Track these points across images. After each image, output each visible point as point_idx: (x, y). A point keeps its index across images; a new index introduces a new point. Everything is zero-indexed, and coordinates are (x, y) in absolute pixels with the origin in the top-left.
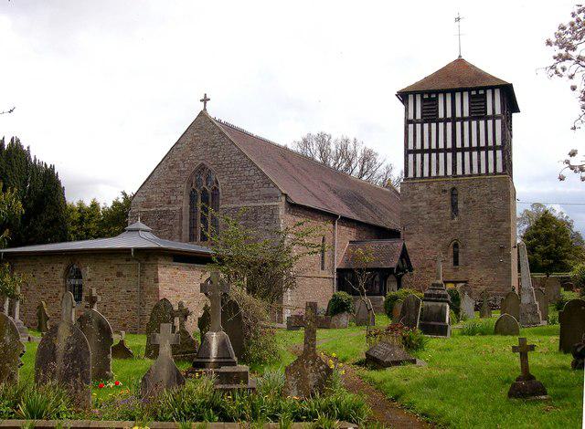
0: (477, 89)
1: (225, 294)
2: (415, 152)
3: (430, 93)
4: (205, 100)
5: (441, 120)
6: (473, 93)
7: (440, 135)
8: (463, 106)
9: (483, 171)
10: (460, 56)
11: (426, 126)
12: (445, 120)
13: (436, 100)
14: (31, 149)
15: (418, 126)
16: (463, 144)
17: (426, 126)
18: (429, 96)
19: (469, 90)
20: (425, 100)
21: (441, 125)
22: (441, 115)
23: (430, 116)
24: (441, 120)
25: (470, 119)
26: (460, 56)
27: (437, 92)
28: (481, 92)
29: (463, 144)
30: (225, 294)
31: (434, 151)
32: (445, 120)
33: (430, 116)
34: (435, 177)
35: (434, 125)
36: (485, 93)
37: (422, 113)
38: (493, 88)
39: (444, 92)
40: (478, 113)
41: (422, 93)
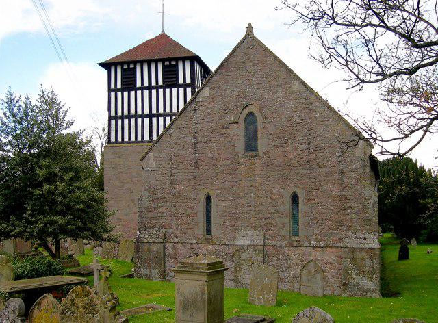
0: (170, 60)
1: (141, 277)
2: (116, 118)
3: (129, 63)
4: (250, 27)
5: (139, 89)
6: (167, 63)
7: (139, 101)
8: (159, 76)
9: (133, 138)
10: (163, 31)
11: (126, 94)
12: (142, 89)
13: (134, 70)
14: (56, 93)
15: (161, 91)
16: (116, 113)
17: (168, 91)
18: (170, 63)
19: (163, 61)
20: (123, 71)
21: (139, 93)
22: (181, 81)
23: (129, 84)
24: (181, 86)
25: (122, 90)
26: (163, 31)
27: (135, 63)
28: (173, 63)
29: (116, 113)
30: (141, 277)
31: (132, 117)
32: (185, 86)
33: (129, 84)
34: (127, 142)
35: (175, 90)
36: (177, 63)
37: (164, 78)
38: (184, 59)
39: (142, 62)
40: (171, 81)
41: (122, 64)
